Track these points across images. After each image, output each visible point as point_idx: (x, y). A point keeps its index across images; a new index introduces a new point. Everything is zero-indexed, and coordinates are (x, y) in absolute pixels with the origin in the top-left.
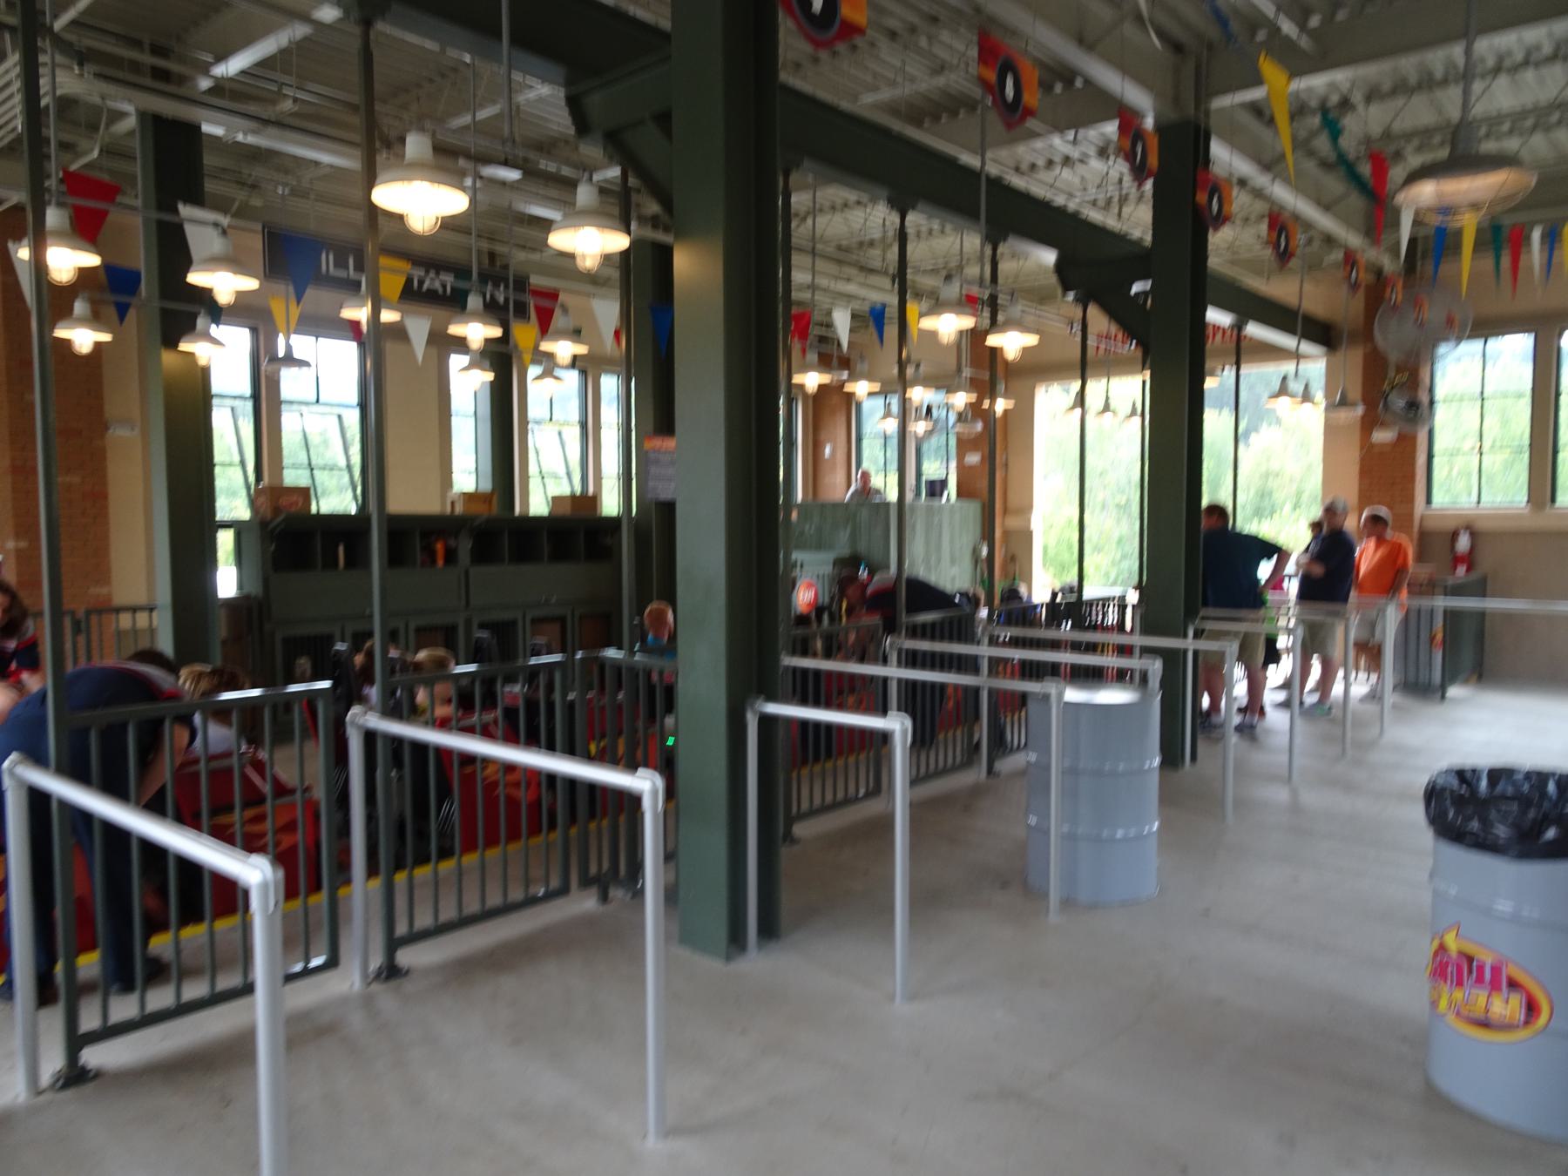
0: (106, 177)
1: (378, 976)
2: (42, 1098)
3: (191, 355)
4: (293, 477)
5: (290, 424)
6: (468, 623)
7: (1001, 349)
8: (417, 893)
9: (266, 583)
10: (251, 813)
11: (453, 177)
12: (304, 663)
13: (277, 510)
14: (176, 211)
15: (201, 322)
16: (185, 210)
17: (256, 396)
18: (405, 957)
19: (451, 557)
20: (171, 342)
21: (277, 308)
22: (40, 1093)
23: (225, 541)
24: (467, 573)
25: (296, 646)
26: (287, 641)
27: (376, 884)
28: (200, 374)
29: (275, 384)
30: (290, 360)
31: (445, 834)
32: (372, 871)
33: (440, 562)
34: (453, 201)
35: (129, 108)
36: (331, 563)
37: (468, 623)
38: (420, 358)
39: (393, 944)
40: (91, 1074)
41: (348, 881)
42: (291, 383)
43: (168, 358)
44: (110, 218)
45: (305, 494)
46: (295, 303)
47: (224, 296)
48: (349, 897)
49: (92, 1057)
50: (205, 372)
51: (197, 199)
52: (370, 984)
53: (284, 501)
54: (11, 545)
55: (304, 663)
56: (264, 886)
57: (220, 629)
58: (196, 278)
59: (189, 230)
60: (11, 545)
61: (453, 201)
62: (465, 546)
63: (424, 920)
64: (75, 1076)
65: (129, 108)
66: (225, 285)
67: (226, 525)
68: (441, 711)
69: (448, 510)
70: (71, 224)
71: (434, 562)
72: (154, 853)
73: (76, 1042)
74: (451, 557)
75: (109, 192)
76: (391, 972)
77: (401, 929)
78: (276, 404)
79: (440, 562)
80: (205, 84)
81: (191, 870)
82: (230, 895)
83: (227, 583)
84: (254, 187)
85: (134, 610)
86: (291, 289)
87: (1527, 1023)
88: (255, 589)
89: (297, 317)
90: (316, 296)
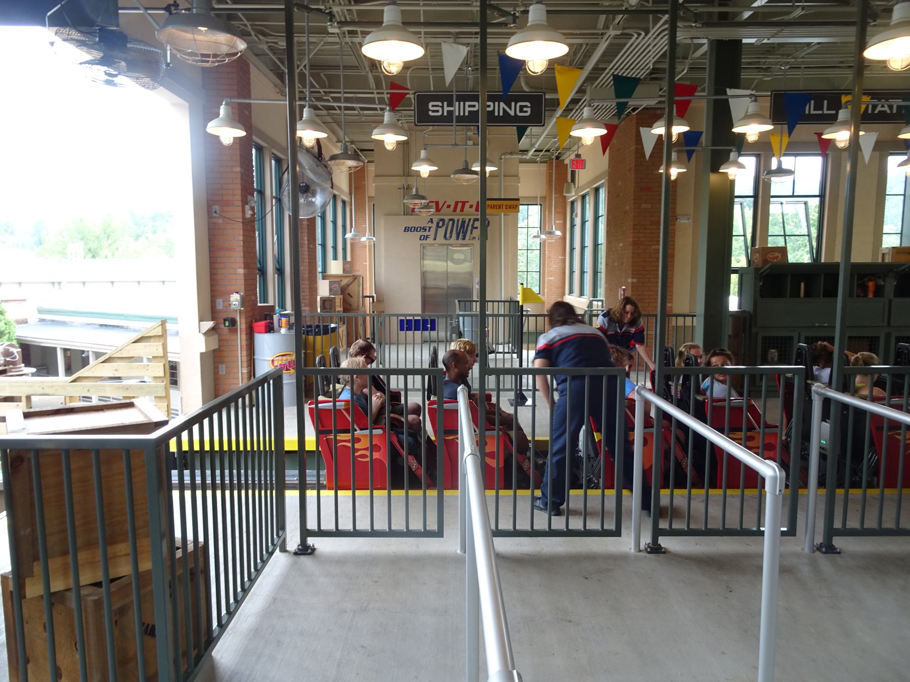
0: (688, 83)
1: (819, 548)
2: (641, 553)
3: (726, 173)
4: (772, 242)
5: (775, 209)
6: (888, 336)
7: (405, 63)
8: (850, 505)
9: (755, 304)
10: (749, 434)
11: (415, 38)
12: (774, 353)
13: (765, 262)
14: (725, 94)
15: (733, 155)
16: (730, 92)
17: (755, 196)
18: (838, 542)
19: (879, 292)
20: (715, 169)
21: (775, 141)
22: (640, 551)
23: (734, 278)
24: (890, 301)
25: (770, 342)
26: (764, 338)
27: (823, 491)
28: (729, 183)
29: (768, 186)
30: (781, 171)
31: (875, 472)
32: (821, 483)
33: (871, 295)
34: (413, 51)
35: (705, 41)
36: (795, 294)
37: (888, 336)
38: (867, 162)
39: (830, 532)
40: (663, 550)
41: (805, 485)
42: (779, 185)
43: (713, 177)
44: (691, 105)
45: (783, 251)
46: (788, 135)
47: (752, 137)
48: (808, 496)
49: (664, 541)
50: (732, 183)
51: (736, 86)
52: (814, 552)
53: (770, 256)
54: (630, 280)
55: (774, 353)
56: (774, 478)
57: (728, 329)
58: (736, 130)
59: (732, 101)
60: (630, 280)
61: (413, 51)
62: (890, 285)
63: (853, 523)
64: (655, 549)
65: (705, 41)
66: (752, 131)
67: (735, 271)
68: (865, 392)
69: (880, 260)
70: (851, 115)
71: (866, 295)
72: (716, 450)
73: (657, 533)
74: (879, 292)
75: (690, 90)
76: (828, 548)
77: (838, 524)
78: (768, 197)
79: (871, 295)
80: (747, 14)
81: (734, 461)
82: (754, 479)
83: (733, 304)
84: (767, 69)
85: (685, 316)
86: (786, 127)
87: (296, 554)
88: (748, 308)
89: (786, 143)
90: (804, 131)
